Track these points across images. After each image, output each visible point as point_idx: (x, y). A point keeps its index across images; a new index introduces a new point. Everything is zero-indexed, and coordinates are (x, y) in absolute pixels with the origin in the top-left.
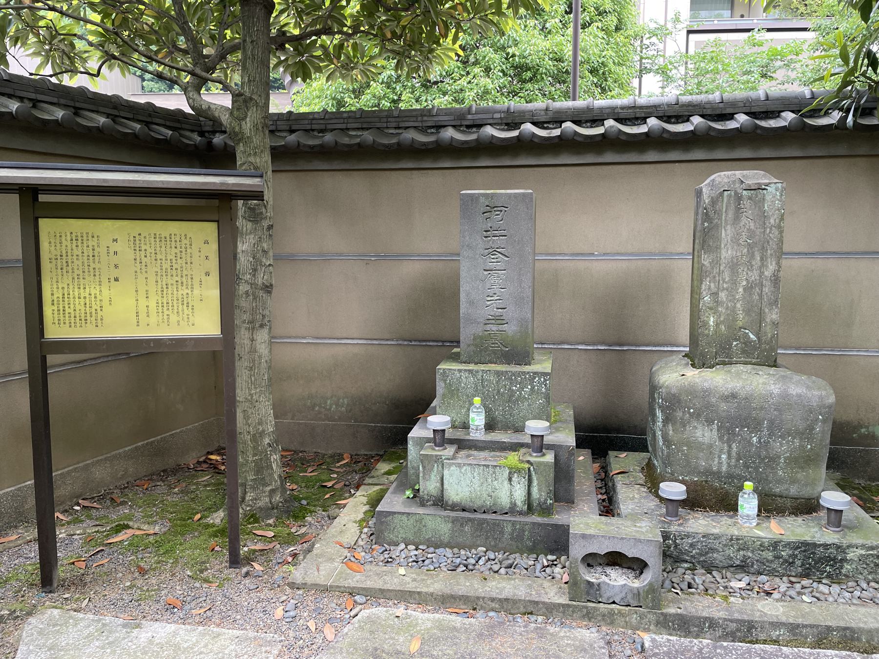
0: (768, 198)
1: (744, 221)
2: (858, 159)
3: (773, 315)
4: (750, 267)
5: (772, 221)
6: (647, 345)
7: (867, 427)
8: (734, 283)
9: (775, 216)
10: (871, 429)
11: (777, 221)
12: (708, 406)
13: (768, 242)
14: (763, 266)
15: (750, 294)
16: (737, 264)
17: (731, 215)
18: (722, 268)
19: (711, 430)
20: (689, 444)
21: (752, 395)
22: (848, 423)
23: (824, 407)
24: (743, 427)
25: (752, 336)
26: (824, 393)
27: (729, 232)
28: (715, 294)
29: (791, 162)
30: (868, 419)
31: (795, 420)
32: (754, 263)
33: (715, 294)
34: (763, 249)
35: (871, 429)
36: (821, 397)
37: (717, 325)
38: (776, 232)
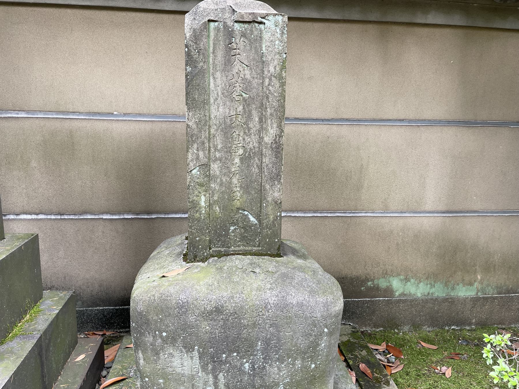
0: (266, 36)
1: (237, 67)
2: (370, 26)
3: (274, 193)
4: (247, 131)
5: (272, 69)
6: (176, 213)
7: (373, 280)
8: (229, 151)
9: (276, 62)
10: (376, 282)
11: (278, 69)
12: (185, 327)
13: (268, 98)
14: (262, 129)
15: (248, 166)
16: (231, 127)
17: (220, 54)
18: (212, 131)
19: (192, 358)
20: (165, 376)
21: (242, 307)
22: (357, 278)
23: (330, 316)
24: (231, 351)
25: (252, 219)
26: (330, 298)
27: (219, 82)
28: (205, 167)
29: (309, 24)
30: (374, 273)
31: (294, 336)
32: (251, 125)
33: (205, 167)
34: (262, 107)
35: (376, 282)
36: (326, 305)
37: (210, 206)
38: (276, 83)
